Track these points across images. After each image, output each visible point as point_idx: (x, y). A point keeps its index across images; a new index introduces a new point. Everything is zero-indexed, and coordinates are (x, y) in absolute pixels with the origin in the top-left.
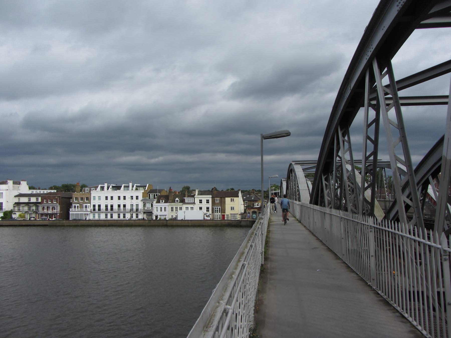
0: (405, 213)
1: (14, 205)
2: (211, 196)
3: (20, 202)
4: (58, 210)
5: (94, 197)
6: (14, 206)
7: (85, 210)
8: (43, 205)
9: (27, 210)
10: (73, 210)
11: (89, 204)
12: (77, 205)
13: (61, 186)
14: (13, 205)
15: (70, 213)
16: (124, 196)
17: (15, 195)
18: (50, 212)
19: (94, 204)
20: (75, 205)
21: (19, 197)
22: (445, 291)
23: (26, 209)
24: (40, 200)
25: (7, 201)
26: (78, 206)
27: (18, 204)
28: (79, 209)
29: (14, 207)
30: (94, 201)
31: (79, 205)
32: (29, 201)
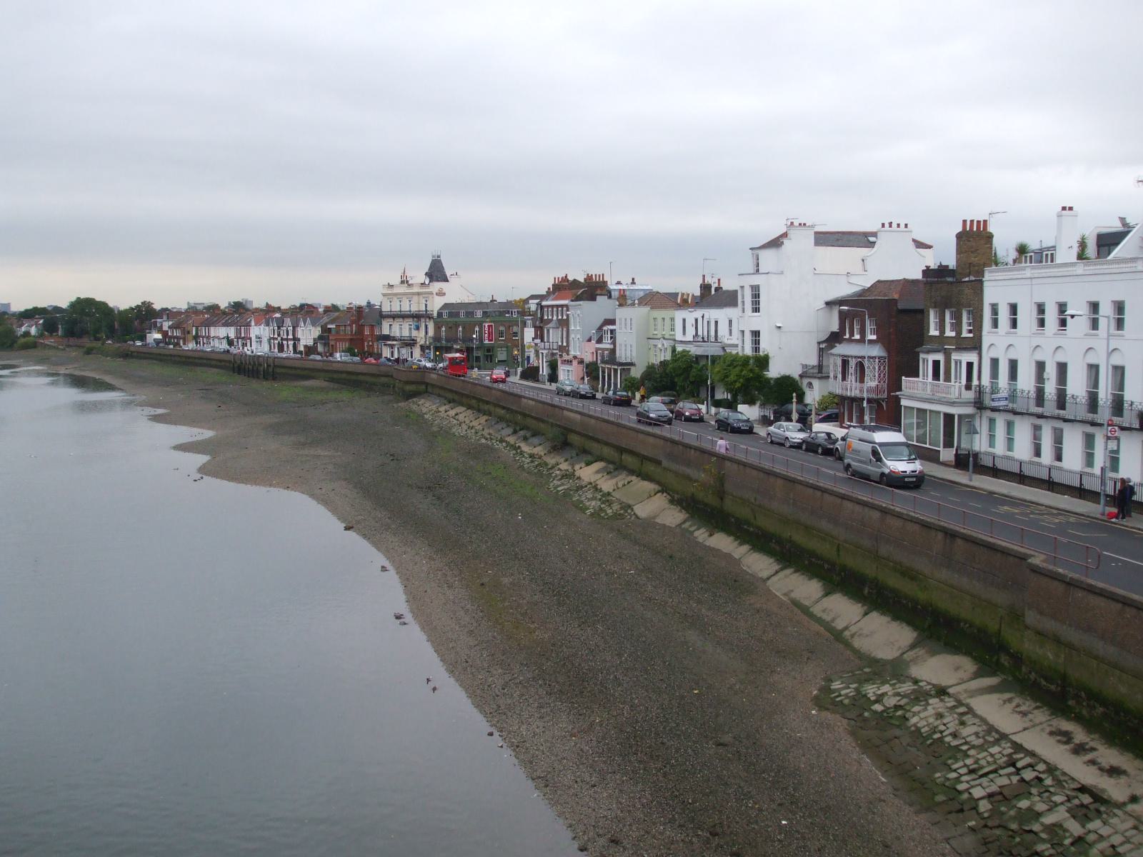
1: (821, 346)
11: (972, 357)
14: (819, 343)
17: (831, 297)
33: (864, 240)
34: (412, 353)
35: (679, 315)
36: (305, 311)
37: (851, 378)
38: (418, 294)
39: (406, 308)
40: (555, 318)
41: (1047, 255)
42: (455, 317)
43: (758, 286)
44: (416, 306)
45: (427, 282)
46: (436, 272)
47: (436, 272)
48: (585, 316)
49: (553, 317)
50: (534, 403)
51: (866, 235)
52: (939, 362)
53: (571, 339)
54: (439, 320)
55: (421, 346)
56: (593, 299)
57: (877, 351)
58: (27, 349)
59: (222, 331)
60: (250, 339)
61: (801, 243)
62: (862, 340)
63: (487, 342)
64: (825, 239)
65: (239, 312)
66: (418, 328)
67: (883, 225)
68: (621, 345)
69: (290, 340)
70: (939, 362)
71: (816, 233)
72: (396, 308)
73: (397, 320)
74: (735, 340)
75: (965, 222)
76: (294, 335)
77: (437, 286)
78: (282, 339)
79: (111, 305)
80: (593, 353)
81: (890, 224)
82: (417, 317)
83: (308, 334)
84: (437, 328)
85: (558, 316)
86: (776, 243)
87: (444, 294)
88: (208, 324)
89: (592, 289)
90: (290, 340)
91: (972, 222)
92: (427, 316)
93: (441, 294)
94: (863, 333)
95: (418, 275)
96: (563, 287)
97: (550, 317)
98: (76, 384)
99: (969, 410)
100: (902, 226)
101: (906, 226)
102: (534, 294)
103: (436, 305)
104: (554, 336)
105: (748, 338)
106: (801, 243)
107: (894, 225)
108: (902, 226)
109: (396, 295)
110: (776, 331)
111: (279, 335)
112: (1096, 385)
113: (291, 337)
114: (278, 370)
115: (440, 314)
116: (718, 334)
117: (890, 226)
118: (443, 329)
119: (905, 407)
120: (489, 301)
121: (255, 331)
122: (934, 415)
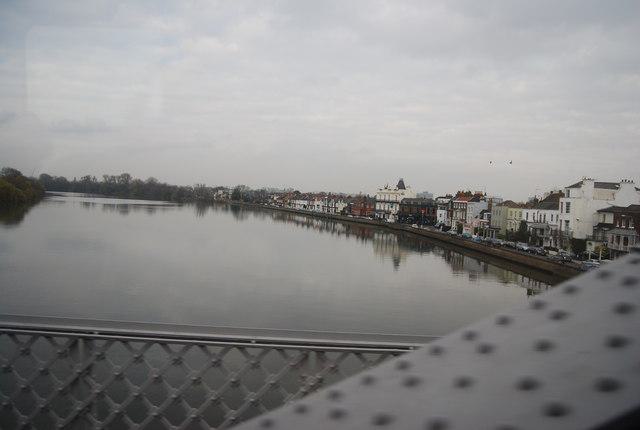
8: (616, 231)
17: (600, 208)
33: (614, 186)
35: (514, 210)
36: (341, 198)
37: (622, 243)
39: (387, 199)
44: (393, 198)
46: (401, 185)
47: (401, 185)
48: (475, 208)
54: (401, 204)
56: (479, 201)
57: (634, 233)
59: (302, 202)
61: (589, 187)
62: (627, 228)
64: (598, 185)
65: (310, 197)
72: (383, 198)
74: (554, 223)
77: (400, 191)
79: (52, 175)
82: (392, 203)
83: (341, 206)
86: (578, 186)
88: (295, 199)
89: (478, 198)
94: (627, 225)
95: (394, 185)
96: (460, 195)
103: (400, 199)
104: (459, 215)
105: (564, 223)
106: (589, 187)
112: (113, 205)
121: (316, 203)
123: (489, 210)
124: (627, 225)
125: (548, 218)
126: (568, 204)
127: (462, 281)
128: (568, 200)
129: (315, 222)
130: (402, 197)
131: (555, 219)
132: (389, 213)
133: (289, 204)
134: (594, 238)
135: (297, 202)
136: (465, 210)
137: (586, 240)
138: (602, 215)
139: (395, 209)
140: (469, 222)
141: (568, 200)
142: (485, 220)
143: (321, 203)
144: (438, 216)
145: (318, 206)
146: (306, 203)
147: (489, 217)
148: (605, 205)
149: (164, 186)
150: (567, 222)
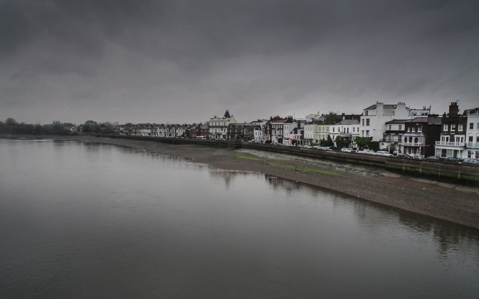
0: (442, 148)
1: (384, 134)
2: (444, 125)
3: (392, 130)
4: (421, 142)
5: (472, 124)
6: (384, 135)
7: (457, 144)
8: (406, 135)
9: (397, 141)
10: (445, 143)
11: (463, 136)
12: (446, 137)
13: (161, 124)
14: (384, 133)
15: (436, 147)
16: (471, 123)
17: (386, 122)
18: (413, 144)
19: (471, 135)
20: (444, 136)
21: (390, 124)
22: (274, 189)
23: (396, 139)
24: (403, 128)
25: (374, 129)
26: (447, 138)
27: (388, 133)
28: (449, 142)
29: (384, 136)
30: (471, 131)
31: (449, 136)
32: (400, 129)
34: (220, 137)
38: (222, 121)
39: (218, 124)
40: (277, 127)
41: (468, 112)
42: (232, 127)
43: (369, 119)
44: (222, 124)
45: (225, 117)
46: (227, 115)
47: (227, 115)
49: (276, 127)
50: (313, 150)
51: (393, 106)
52: (448, 137)
53: (284, 133)
54: (229, 127)
55: (223, 135)
58: (99, 137)
59: (146, 131)
60: (157, 133)
63: (245, 134)
65: (152, 127)
66: (222, 130)
67: (399, 103)
68: (306, 135)
69: (174, 133)
70: (448, 137)
71: (384, 105)
72: (214, 124)
73: (218, 128)
74: (356, 132)
75: (452, 103)
76: (175, 132)
77: (227, 119)
78: (171, 133)
80: (294, 137)
81: (400, 103)
84: (228, 130)
85: (278, 127)
87: (230, 121)
90: (174, 133)
91: (453, 103)
92: (225, 127)
93: (229, 121)
95: (222, 115)
96: (272, 120)
97: (275, 127)
98: (87, 144)
99: (462, 149)
100: (403, 103)
101: (404, 103)
102: (254, 121)
103: (227, 124)
105: (365, 132)
107: (401, 103)
108: (403, 103)
109: (214, 121)
110: (374, 131)
111: (169, 132)
113: (174, 132)
114: (179, 141)
115: (229, 126)
116: (349, 131)
117: (400, 103)
118: (236, 130)
119: (436, 149)
120: (244, 123)
122: (449, 151)
123: (299, 127)
124: (416, 130)
125: (351, 131)
126: (368, 120)
127: (281, 192)
128: (367, 117)
129: (307, 146)
130: (229, 123)
131: (356, 130)
132: (219, 134)
133: (135, 133)
134: (384, 140)
135: (142, 131)
136: (283, 129)
137: (380, 142)
138: (388, 126)
139: (224, 132)
140: (286, 136)
141: (367, 117)
142: (299, 134)
143: (162, 130)
144: (255, 134)
145: (161, 133)
146: (149, 131)
147: (302, 132)
148: (389, 119)
149: (22, 125)
150: (368, 131)
